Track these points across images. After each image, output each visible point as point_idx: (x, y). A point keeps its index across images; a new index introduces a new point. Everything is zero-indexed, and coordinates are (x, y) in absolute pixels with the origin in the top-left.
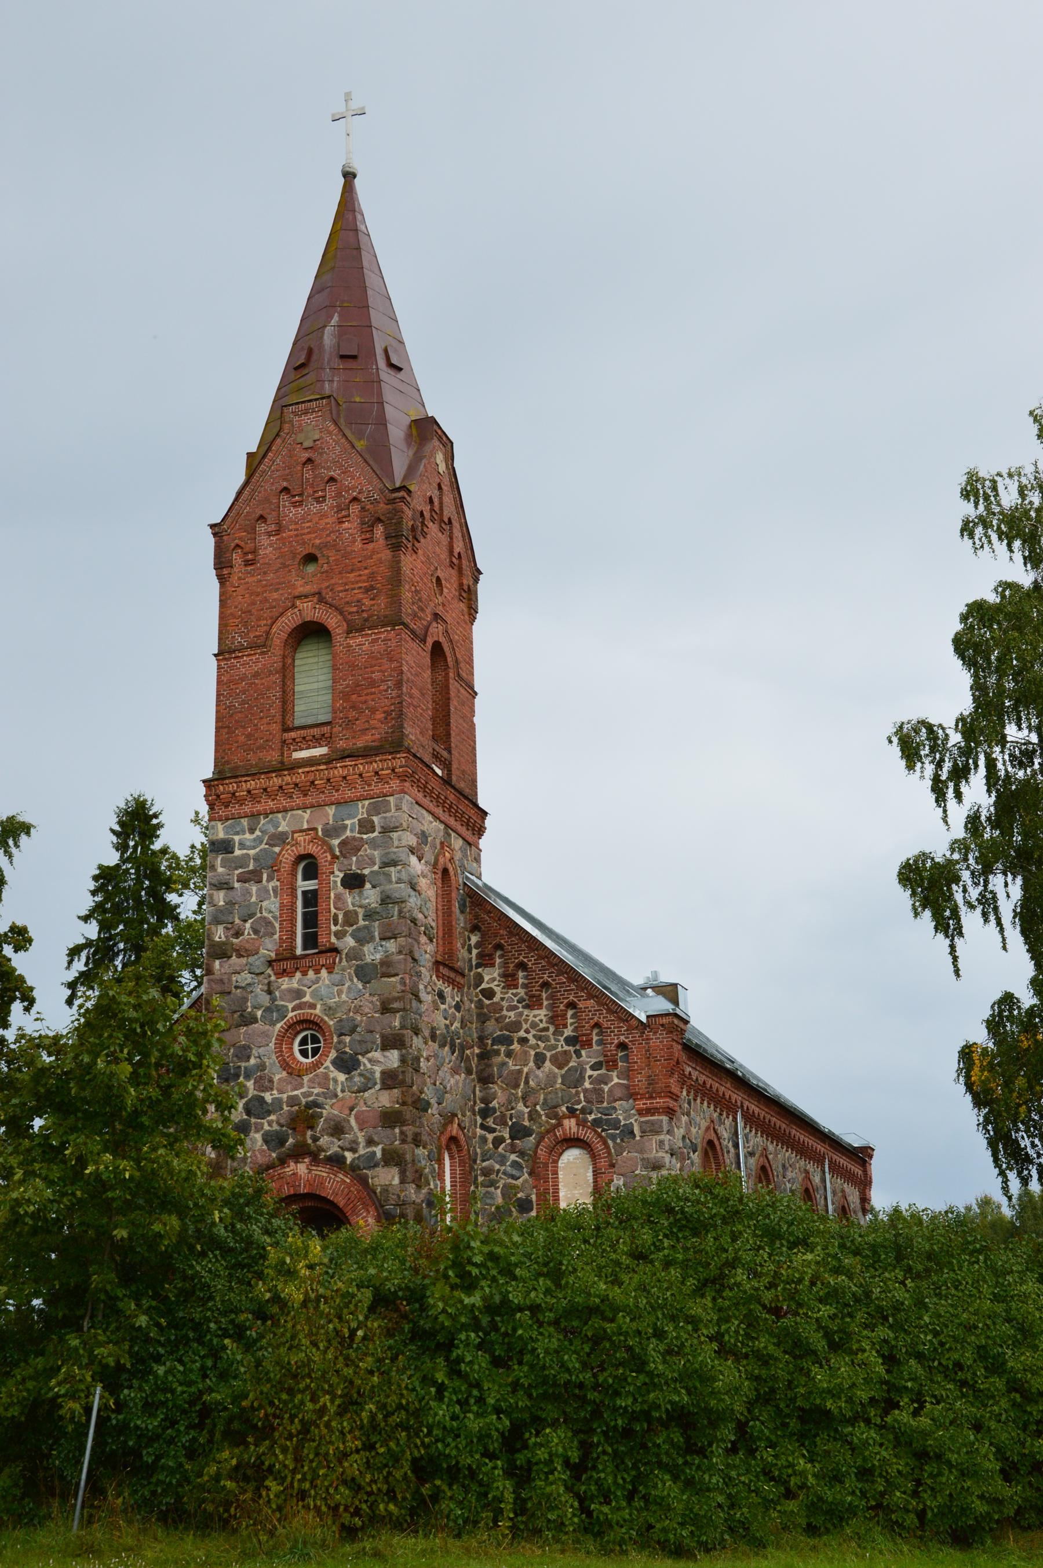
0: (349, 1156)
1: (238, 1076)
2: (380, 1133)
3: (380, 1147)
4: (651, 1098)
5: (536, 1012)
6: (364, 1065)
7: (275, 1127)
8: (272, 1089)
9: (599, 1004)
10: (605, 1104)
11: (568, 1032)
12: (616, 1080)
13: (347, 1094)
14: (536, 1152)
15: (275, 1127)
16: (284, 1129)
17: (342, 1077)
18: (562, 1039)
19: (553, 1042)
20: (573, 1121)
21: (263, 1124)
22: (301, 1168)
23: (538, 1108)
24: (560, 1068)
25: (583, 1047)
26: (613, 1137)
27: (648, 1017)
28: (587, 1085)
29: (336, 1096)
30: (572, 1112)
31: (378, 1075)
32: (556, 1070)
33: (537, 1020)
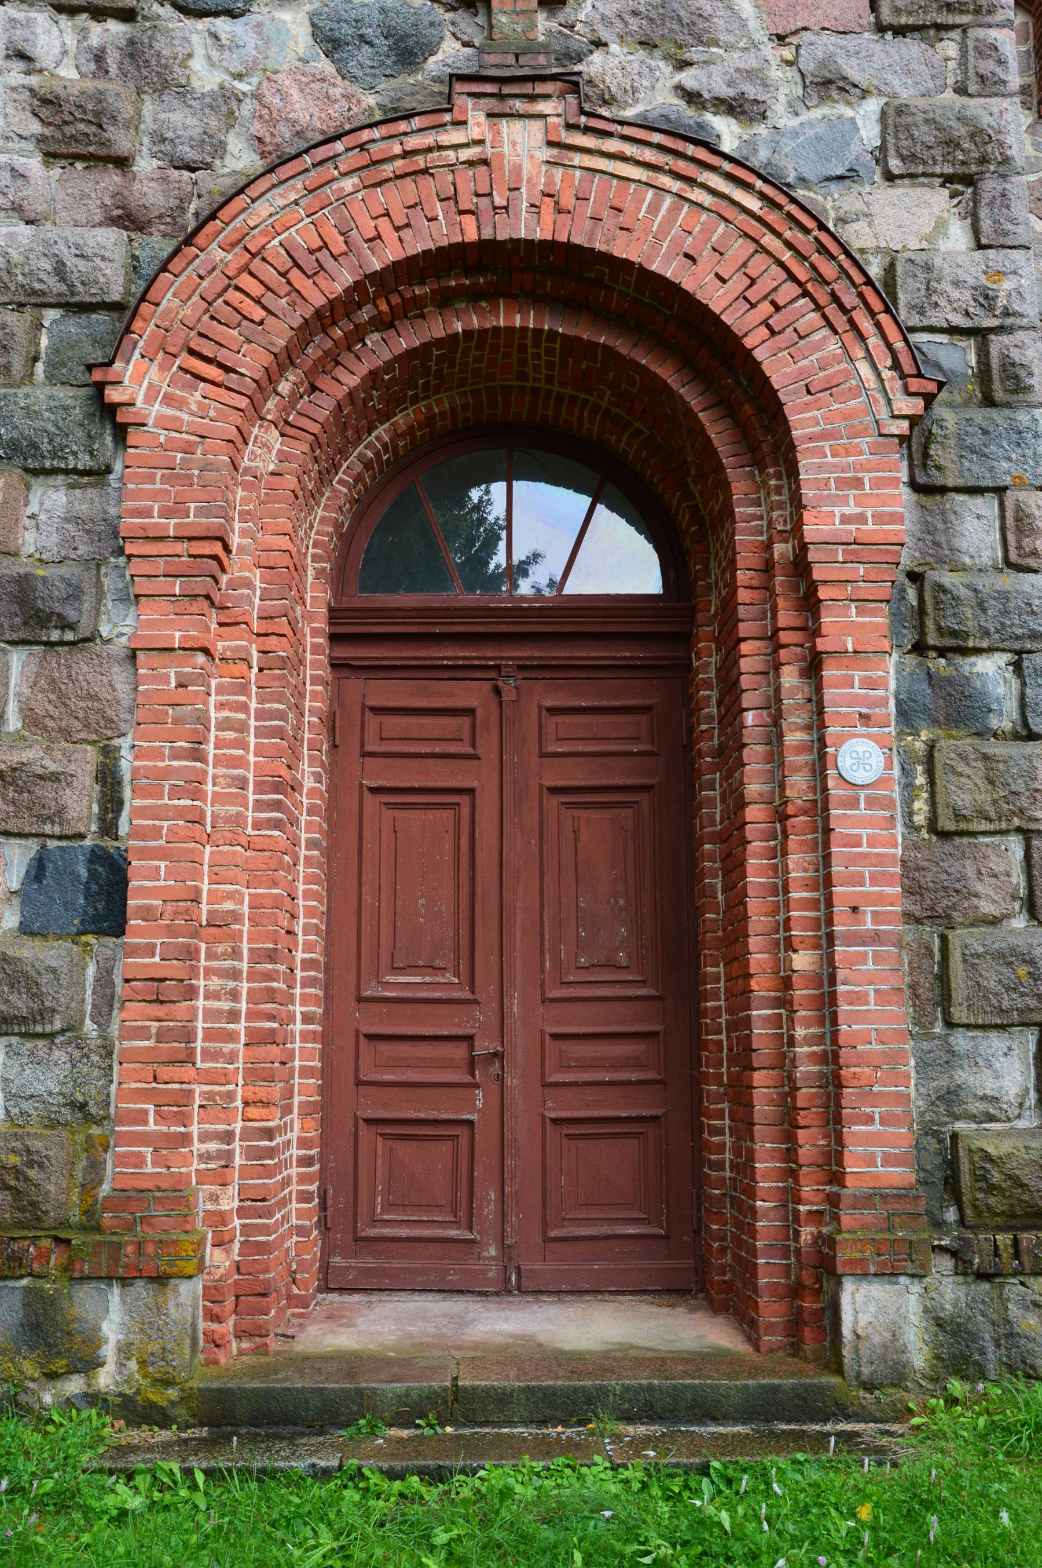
0: (728, 133)
3: (873, 106)
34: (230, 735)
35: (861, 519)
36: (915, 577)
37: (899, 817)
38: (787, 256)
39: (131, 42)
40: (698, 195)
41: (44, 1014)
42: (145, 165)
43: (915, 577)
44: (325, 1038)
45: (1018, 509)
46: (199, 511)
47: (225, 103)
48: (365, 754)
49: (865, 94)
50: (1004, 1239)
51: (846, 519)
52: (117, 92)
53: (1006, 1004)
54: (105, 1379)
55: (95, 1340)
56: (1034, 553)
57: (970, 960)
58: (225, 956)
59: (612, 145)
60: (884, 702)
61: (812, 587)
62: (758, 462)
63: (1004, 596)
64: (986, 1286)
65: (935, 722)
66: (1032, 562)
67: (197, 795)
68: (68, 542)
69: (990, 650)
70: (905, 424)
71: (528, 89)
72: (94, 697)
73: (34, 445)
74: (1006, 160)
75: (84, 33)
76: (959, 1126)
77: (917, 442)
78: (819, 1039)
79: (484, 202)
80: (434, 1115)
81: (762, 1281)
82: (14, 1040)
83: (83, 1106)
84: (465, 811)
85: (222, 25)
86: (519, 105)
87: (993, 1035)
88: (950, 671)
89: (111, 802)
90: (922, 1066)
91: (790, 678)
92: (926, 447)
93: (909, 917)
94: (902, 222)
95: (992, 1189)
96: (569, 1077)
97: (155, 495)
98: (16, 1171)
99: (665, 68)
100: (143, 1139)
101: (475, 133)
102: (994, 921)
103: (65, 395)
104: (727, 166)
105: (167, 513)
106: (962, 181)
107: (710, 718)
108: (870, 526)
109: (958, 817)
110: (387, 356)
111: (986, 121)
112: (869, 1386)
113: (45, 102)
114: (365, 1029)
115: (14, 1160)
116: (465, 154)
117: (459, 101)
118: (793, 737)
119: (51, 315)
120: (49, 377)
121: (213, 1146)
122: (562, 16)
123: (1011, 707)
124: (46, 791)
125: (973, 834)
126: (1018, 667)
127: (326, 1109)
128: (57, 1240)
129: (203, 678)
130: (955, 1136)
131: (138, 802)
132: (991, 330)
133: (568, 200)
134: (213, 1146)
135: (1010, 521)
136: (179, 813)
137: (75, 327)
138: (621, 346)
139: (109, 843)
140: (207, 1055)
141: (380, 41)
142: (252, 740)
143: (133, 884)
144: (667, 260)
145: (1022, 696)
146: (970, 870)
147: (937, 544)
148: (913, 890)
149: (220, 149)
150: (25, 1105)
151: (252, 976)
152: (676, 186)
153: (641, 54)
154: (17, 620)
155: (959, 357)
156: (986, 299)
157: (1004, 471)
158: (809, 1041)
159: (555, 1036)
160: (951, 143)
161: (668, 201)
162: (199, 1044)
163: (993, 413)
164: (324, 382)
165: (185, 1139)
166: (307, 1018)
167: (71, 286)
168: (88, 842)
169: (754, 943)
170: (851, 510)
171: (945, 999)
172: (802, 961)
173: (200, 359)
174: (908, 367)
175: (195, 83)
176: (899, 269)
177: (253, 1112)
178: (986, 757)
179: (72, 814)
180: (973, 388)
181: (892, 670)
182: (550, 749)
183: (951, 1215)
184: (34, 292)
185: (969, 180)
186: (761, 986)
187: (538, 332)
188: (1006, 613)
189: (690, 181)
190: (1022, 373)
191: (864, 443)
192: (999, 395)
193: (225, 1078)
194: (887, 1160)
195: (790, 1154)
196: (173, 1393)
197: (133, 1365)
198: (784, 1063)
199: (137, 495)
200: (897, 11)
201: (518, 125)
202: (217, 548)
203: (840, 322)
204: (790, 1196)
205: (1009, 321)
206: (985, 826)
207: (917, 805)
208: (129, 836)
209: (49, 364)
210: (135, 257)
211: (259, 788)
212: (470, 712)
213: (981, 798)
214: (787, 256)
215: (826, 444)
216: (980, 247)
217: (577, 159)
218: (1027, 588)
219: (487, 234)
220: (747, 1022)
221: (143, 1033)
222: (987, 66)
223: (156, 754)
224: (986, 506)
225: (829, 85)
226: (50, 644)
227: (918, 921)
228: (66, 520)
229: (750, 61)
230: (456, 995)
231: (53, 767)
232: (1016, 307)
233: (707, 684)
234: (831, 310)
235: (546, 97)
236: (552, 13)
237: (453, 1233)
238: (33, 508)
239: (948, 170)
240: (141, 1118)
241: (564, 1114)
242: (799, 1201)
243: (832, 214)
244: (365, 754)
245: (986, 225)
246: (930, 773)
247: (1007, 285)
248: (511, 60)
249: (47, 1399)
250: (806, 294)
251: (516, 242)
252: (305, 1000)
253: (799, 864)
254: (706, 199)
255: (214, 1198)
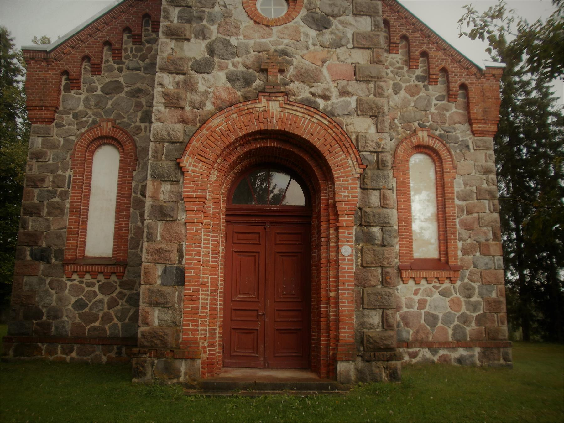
0: (322, 103)
1: (201, 19)
2: (354, 86)
3: (355, 98)
4: (485, 123)
5: (394, 55)
6: (336, 25)
7: (241, 68)
8: (237, 34)
9: (445, 54)
10: (447, 125)
11: (419, 72)
12: (454, 110)
13: (319, 48)
14: (395, 152)
15: (241, 68)
16: (251, 70)
17: (313, 33)
18: (414, 76)
19: (407, 77)
20: (425, 134)
21: (228, 64)
22: (274, 107)
23: (396, 121)
24: (412, 95)
25: (430, 83)
26: (455, 148)
27: (486, 67)
28: (433, 110)
29: (307, 48)
30: (422, 127)
31: (350, 36)
32: (409, 97)
33: (394, 61)
34: (206, 242)
35: (348, 196)
36: (360, 209)
37: (354, 263)
38: (334, 135)
39: (185, 80)
40: (314, 120)
41: (167, 303)
42: (188, 108)
43: (360, 209)
44: (224, 309)
45: (384, 194)
46: (201, 192)
47: (206, 93)
48: (233, 243)
49: (353, 95)
50: (372, 354)
51: (345, 196)
52: (181, 91)
53: (375, 304)
54: (182, 379)
55: (179, 371)
56: (387, 204)
57: (368, 295)
58: (206, 291)
59: (295, 108)
60: (352, 237)
61: (337, 212)
62: (327, 180)
63: (379, 214)
64: (368, 363)
65: (363, 242)
66: (386, 206)
67: (200, 255)
68: (171, 197)
69: (376, 226)
70: (359, 175)
71: (276, 95)
72: (177, 233)
73: (163, 175)
74: (384, 113)
75: (174, 78)
76: (365, 330)
77: (362, 178)
78: (335, 311)
79: (265, 120)
80: (249, 328)
81: (322, 363)
82: (160, 308)
83: (175, 323)
84: (257, 257)
85: (205, 75)
86: (273, 98)
87: (373, 311)
88: (367, 230)
89: (181, 257)
90: (357, 317)
91: (332, 231)
92: (364, 179)
93: (355, 285)
94: (362, 126)
95: (371, 343)
96: (280, 320)
97: (191, 188)
98: (162, 336)
99: (307, 87)
100: (189, 330)
101: (263, 104)
102: (374, 286)
103: (170, 163)
104: (321, 114)
105: (193, 192)
106: (375, 116)
107: (315, 237)
108: (350, 198)
109: (367, 263)
110: (242, 153)
111: (379, 104)
112: (342, 383)
113: (166, 95)
114: (233, 308)
115: (161, 334)
116: (261, 109)
117: (260, 97)
118: (332, 245)
119: (166, 144)
120: (166, 158)
121: (203, 332)
122: (284, 75)
123: (380, 239)
124: (167, 254)
125: (371, 267)
126: (382, 229)
127: (224, 326)
128: (171, 351)
129: (201, 230)
130: (363, 332)
131: (187, 257)
132: (379, 152)
133: (285, 120)
134: (203, 332)
135: (382, 197)
136: (196, 259)
137: (171, 147)
138: (296, 151)
139: (180, 266)
140: (202, 312)
141: (242, 80)
142: (211, 242)
143: (186, 275)
144: (307, 135)
145: (383, 237)
146: (370, 275)
147: (366, 201)
148: (357, 279)
149: (205, 105)
150: (163, 322)
151: (211, 295)
152: (309, 117)
153: (302, 84)
154: (160, 215)
155: (373, 158)
156: (378, 145)
157: (381, 185)
158: (333, 311)
159: (277, 310)
160: (372, 109)
161: (307, 121)
162: (200, 310)
163: (379, 171)
164: (227, 159)
165: (197, 330)
166: (221, 305)
167: (171, 138)
168: (176, 265)
169: (322, 290)
170: (346, 194)
171: (363, 303)
172: (332, 294)
173: (201, 156)
174: (360, 162)
175: (199, 89)
176: (359, 137)
177: (211, 325)
178: (374, 250)
179: (173, 259)
180: (375, 165)
181: (354, 230)
182: (277, 243)
183: (362, 349)
184: (163, 139)
185: (376, 116)
186: (323, 300)
187: (277, 147)
188: (380, 218)
189: (312, 117)
190: (386, 163)
191: (349, 179)
192: (381, 167)
193: (205, 317)
194: (349, 337)
195: (328, 336)
196: (196, 383)
197: (187, 377)
198: (328, 316)
199: (187, 188)
200: (360, 77)
201: (273, 102)
202: (204, 200)
203: (345, 150)
204: (328, 345)
205: (383, 150)
206: (373, 265)
207: (359, 260)
208: (185, 264)
209: (166, 156)
210: (185, 130)
211: (212, 253)
212: (259, 233)
213: (372, 259)
214: (334, 135)
215: (341, 179)
216: (378, 132)
217: (287, 111)
218: (385, 212)
219: (266, 128)
220: (320, 307)
221: (188, 307)
222: (380, 91)
223: (191, 246)
224: (377, 193)
225: (344, 93)
226: (167, 221)
227: (358, 286)
228: (170, 192)
229: (327, 87)
230: (254, 300)
231: (168, 249)
232: (385, 147)
233: (315, 229)
234: (343, 147)
235: (280, 96)
236: (281, 74)
237: (253, 355)
238: (162, 189)
239: (371, 114)
240: (188, 325)
241: (279, 328)
242: (330, 346)
243: (345, 123)
244: (233, 243)
245: (379, 127)
246: (361, 253)
247: (383, 142)
248: (272, 87)
249: (169, 383)
250: (338, 143)
251: (272, 130)
252: (220, 301)
253: (332, 273)
254: (316, 121)
255: (203, 343)
